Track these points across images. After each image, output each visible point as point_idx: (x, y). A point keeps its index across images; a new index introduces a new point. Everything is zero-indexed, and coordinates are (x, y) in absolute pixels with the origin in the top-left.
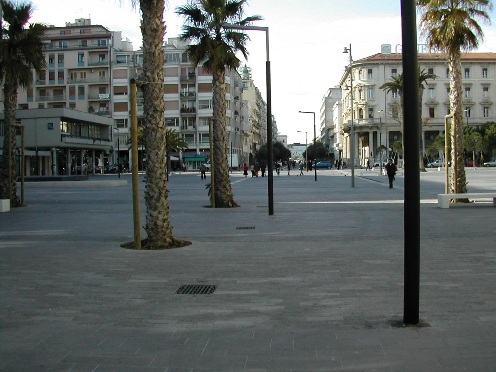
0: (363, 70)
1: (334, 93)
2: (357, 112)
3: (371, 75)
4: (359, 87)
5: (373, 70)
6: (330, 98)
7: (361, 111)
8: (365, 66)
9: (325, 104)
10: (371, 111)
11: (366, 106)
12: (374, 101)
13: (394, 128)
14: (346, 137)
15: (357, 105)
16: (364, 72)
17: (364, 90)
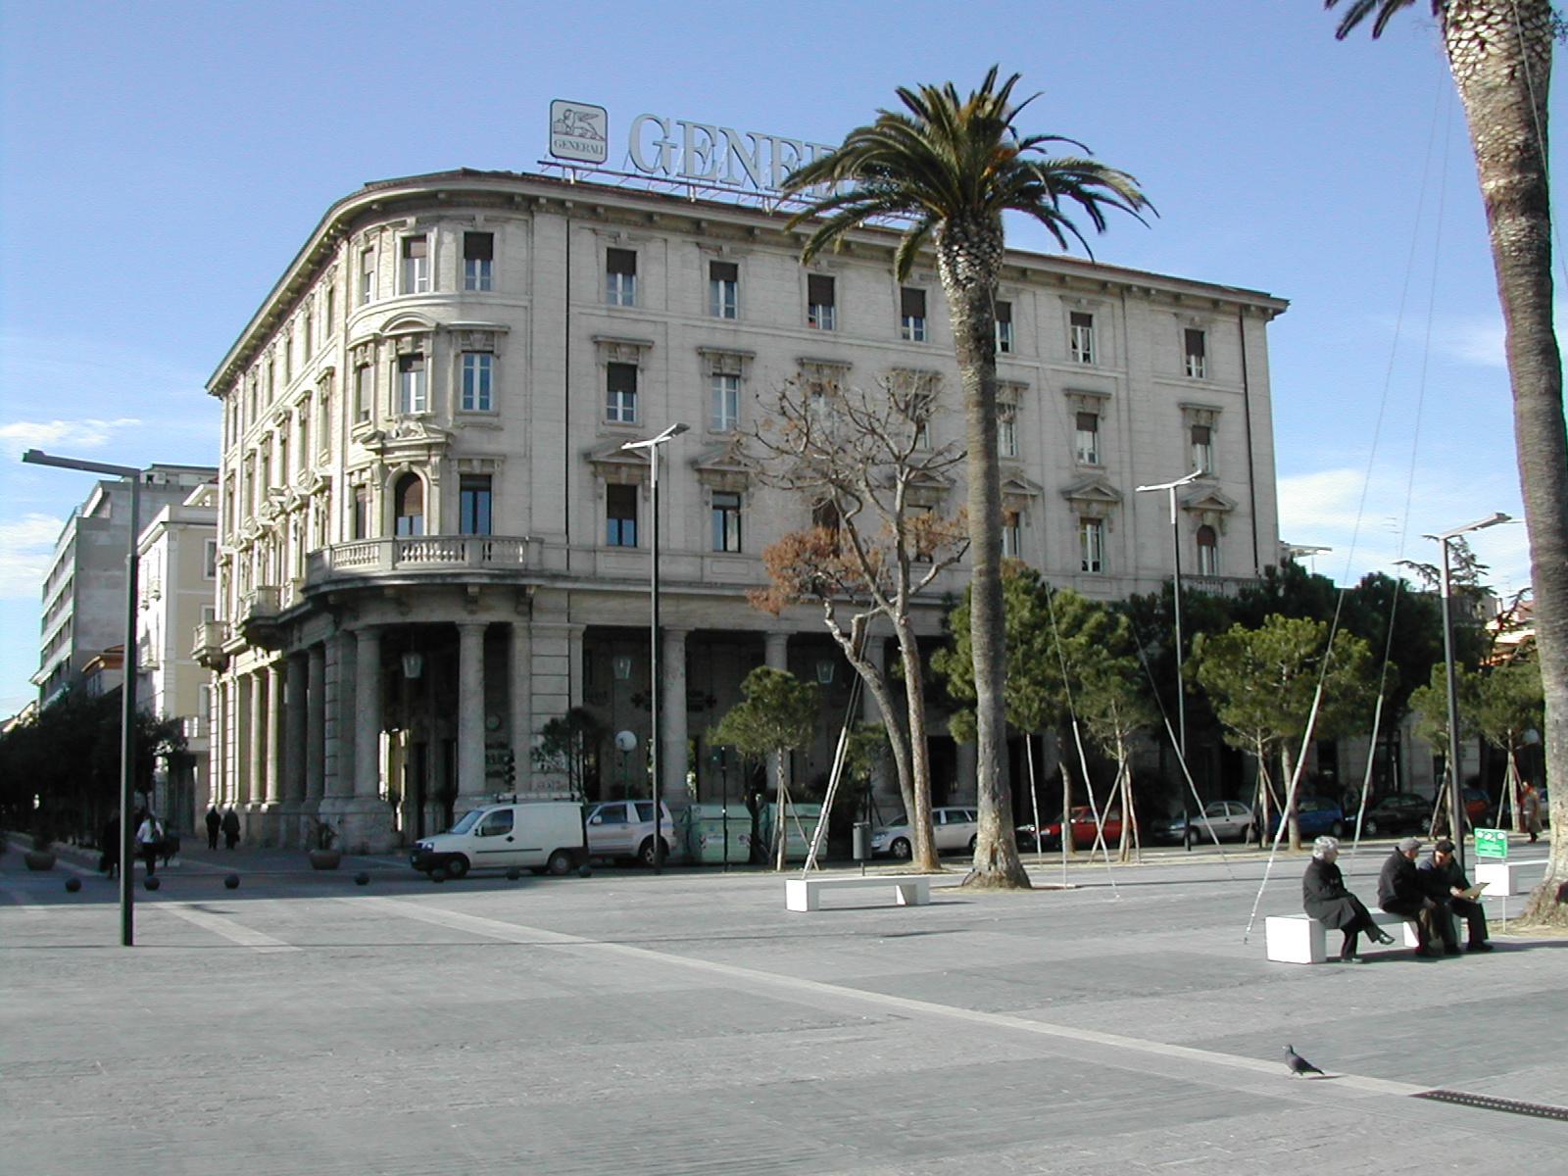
0: (432, 236)
1: (121, 503)
2: (376, 494)
3: (486, 270)
4: (398, 338)
5: (496, 237)
6: (103, 525)
7: (410, 492)
8: (451, 212)
9: (78, 543)
10: (475, 491)
11: (444, 457)
12: (499, 429)
13: (614, 604)
14: (245, 680)
15: (382, 451)
16: (439, 243)
17: (434, 355)
